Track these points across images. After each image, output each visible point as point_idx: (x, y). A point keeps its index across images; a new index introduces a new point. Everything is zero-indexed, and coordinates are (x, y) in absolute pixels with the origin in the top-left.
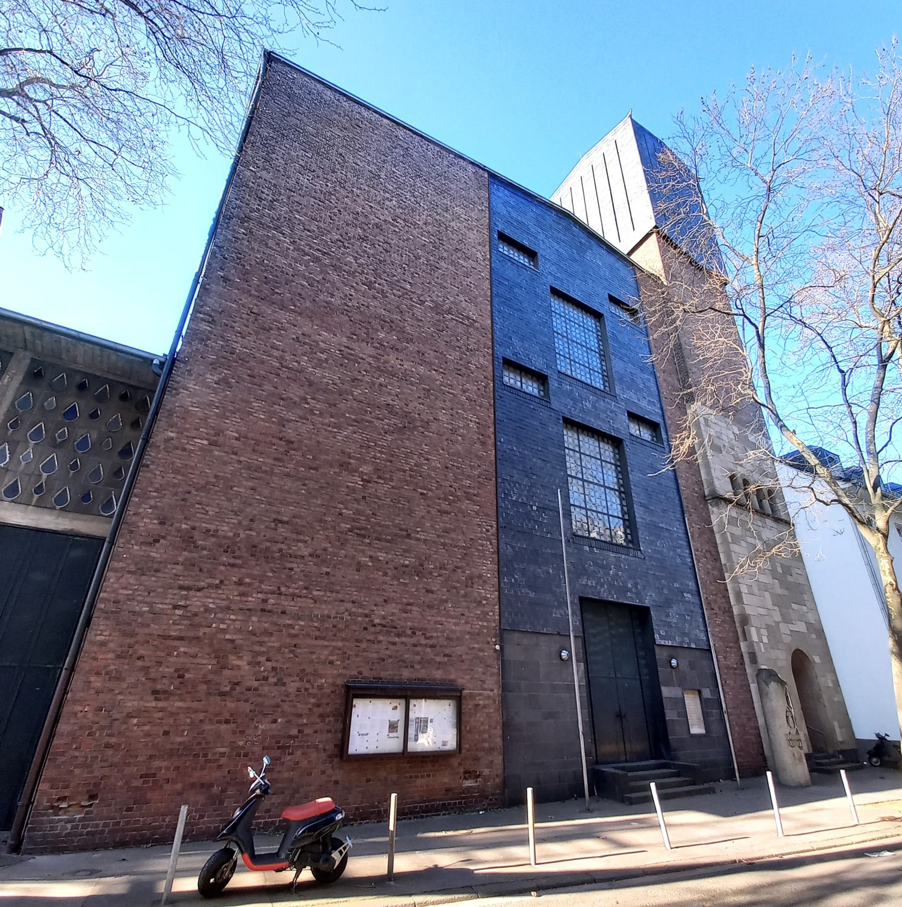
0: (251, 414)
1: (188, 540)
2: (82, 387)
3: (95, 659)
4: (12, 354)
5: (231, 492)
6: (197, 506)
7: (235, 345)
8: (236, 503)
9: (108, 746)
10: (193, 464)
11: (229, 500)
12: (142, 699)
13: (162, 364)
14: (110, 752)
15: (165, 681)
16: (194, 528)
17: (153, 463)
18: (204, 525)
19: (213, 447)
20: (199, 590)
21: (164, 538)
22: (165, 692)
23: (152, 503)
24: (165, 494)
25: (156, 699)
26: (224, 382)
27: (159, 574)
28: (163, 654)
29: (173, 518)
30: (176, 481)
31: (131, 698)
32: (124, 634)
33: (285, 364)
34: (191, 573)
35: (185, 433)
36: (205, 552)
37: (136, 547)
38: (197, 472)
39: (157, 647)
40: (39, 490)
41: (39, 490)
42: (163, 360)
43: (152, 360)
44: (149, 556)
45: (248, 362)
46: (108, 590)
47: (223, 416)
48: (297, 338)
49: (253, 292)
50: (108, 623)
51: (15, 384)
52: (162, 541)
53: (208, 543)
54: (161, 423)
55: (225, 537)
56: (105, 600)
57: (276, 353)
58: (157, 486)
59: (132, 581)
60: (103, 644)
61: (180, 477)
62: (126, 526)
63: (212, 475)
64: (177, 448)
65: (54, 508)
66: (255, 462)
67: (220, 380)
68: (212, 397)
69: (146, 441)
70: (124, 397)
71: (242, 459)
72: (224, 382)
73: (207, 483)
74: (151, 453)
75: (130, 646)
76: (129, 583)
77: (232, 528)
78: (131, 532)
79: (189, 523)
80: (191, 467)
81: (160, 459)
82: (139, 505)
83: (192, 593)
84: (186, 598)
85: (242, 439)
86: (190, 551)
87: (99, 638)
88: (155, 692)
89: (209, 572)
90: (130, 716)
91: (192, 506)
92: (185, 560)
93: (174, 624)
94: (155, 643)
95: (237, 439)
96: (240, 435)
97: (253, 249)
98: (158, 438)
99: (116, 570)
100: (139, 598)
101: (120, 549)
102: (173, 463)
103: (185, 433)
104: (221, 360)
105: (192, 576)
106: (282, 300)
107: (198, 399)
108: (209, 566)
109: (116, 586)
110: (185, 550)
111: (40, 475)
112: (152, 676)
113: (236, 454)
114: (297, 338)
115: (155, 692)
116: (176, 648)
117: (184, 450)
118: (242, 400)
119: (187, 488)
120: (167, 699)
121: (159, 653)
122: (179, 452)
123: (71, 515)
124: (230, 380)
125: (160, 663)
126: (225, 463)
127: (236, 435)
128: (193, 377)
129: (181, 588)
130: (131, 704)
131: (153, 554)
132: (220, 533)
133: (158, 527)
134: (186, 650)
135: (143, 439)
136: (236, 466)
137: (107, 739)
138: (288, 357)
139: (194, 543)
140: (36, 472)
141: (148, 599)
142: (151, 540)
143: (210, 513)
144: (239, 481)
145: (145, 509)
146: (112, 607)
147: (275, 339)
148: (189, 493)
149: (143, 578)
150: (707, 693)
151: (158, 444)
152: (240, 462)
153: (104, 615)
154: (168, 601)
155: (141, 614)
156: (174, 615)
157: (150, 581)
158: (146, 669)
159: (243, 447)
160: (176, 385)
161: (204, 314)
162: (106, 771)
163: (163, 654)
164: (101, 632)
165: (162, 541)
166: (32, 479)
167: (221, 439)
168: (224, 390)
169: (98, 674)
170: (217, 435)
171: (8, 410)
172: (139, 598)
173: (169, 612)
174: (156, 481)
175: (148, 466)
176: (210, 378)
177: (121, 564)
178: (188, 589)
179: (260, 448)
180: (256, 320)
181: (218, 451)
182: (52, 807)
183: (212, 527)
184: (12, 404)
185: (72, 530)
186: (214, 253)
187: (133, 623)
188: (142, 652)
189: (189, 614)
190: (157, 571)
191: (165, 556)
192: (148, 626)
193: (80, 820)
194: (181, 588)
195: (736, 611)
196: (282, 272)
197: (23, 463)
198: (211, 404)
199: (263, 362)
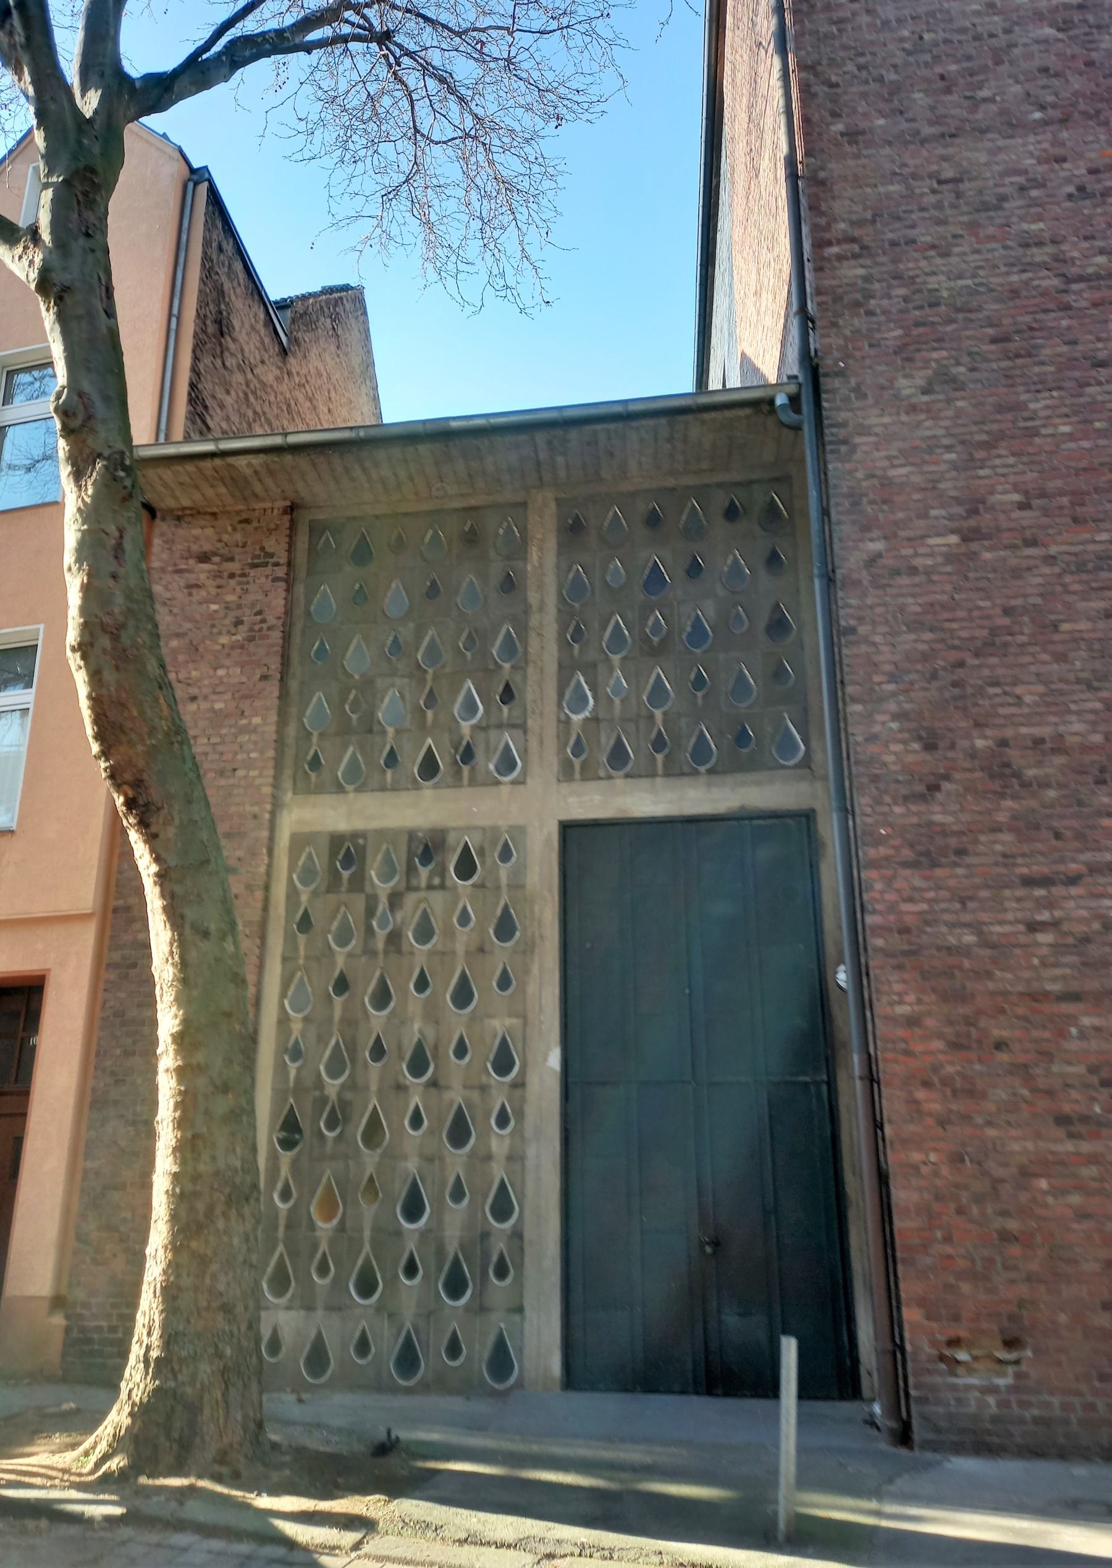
0: (1033, 433)
1: (1001, 772)
2: (653, 520)
3: (908, 1053)
4: (524, 505)
5: (1056, 637)
6: (992, 690)
7: (932, 282)
8: (1080, 660)
9: (1006, 1237)
10: (945, 598)
11: (1061, 658)
12: (1038, 1136)
13: (794, 401)
14: (1015, 1250)
15: (1074, 1094)
16: (1003, 743)
17: (861, 619)
18: (1024, 730)
19: (974, 546)
20: (1073, 880)
21: (947, 777)
22: (1085, 1119)
23: (892, 706)
24: (912, 683)
25: (1071, 1136)
26: (944, 379)
27: (969, 860)
28: (1047, 1034)
29: (950, 730)
30: (922, 647)
31: (1014, 1132)
32: (945, 997)
33: (1074, 271)
34: (1039, 846)
35: (903, 534)
36: (1052, 794)
37: (897, 810)
38: (961, 614)
39: (1026, 1019)
40: (659, 744)
41: (659, 744)
42: (792, 389)
43: (771, 401)
44: (931, 824)
45: (980, 309)
46: (878, 907)
47: (970, 464)
48: (1081, 189)
49: (927, 131)
50: (906, 976)
51: (551, 559)
52: (946, 786)
53: (1048, 770)
54: (844, 528)
55: (1086, 749)
56: (879, 930)
57: (1040, 255)
58: (888, 668)
59: (918, 882)
60: (912, 1021)
61: (929, 636)
62: (862, 769)
63: (998, 611)
64: (897, 572)
65: (695, 773)
66: (1090, 547)
67: (930, 382)
68: (929, 429)
69: (830, 580)
70: (731, 513)
71: (1053, 550)
72: (944, 379)
73: (994, 631)
74: (849, 601)
75: (969, 1022)
76: (915, 889)
77: (1094, 723)
78: (875, 779)
79: (989, 732)
80: (944, 607)
81: (871, 607)
82: (869, 717)
83: (1058, 891)
84: (1050, 905)
85: (1036, 502)
86: (1015, 797)
87: (900, 1010)
88: (1062, 1120)
89: (1080, 836)
90: (1026, 1174)
91: (980, 692)
92: (1014, 818)
93: (1044, 964)
94: (1020, 1011)
95: (1023, 506)
96: (1026, 493)
97: (886, 23)
98: (851, 561)
99: (874, 864)
100: (947, 917)
101: (869, 820)
102: (902, 609)
103: (903, 534)
104: (916, 332)
105: (1042, 854)
106: (1003, 112)
107: (900, 444)
108: (1074, 823)
109: (890, 897)
110: (1002, 795)
111: (651, 717)
112: (1042, 1083)
113: (1033, 543)
114: (1081, 189)
115: (1062, 1120)
116: (1072, 1019)
117: (913, 571)
118: (1000, 409)
119: (954, 656)
120: (1095, 1136)
121: (1036, 1034)
122: (905, 580)
123: (729, 779)
124: (954, 370)
125: (1047, 1056)
126: (1017, 573)
127: (1016, 497)
128: (870, 401)
129: (1029, 882)
130: (1020, 1146)
131: (938, 818)
132: (1071, 740)
133: (927, 756)
134: (1096, 1021)
135: (821, 576)
136: (1047, 570)
137: (998, 1223)
138: (1072, 250)
139: (1017, 775)
140: (643, 712)
141: (967, 918)
142: (920, 788)
143: (1028, 699)
144: (1068, 606)
145: (883, 723)
146: (899, 943)
147: (1022, 219)
148: (961, 664)
149: (938, 872)
151: (855, 576)
152: (1050, 560)
153: (893, 961)
154: (1010, 916)
155: (964, 951)
156: (1038, 944)
157: (953, 876)
158: (1022, 1070)
159: (1044, 520)
160: (842, 433)
161: (839, 242)
162: (1023, 1290)
163: (1047, 1034)
164: (898, 998)
165: (946, 786)
166: (642, 726)
167: (986, 520)
168: (949, 401)
169: (927, 1084)
170: (974, 512)
171: (559, 611)
172: (947, 917)
173: (1023, 939)
174: (881, 658)
175: (852, 630)
176: (907, 386)
177: (883, 851)
178: (1046, 882)
179: (1088, 510)
180: (959, 195)
181: (988, 550)
182: (942, 1358)
183: (1045, 731)
184: (561, 599)
185: (742, 808)
186: (806, 90)
187: (957, 972)
188: (996, 1033)
189: (1070, 940)
190: (961, 852)
191: (965, 817)
192: (989, 975)
193: (1011, 1389)
194: (1029, 882)
196: (977, 38)
197: (617, 701)
198: (932, 446)
199: (1015, 293)
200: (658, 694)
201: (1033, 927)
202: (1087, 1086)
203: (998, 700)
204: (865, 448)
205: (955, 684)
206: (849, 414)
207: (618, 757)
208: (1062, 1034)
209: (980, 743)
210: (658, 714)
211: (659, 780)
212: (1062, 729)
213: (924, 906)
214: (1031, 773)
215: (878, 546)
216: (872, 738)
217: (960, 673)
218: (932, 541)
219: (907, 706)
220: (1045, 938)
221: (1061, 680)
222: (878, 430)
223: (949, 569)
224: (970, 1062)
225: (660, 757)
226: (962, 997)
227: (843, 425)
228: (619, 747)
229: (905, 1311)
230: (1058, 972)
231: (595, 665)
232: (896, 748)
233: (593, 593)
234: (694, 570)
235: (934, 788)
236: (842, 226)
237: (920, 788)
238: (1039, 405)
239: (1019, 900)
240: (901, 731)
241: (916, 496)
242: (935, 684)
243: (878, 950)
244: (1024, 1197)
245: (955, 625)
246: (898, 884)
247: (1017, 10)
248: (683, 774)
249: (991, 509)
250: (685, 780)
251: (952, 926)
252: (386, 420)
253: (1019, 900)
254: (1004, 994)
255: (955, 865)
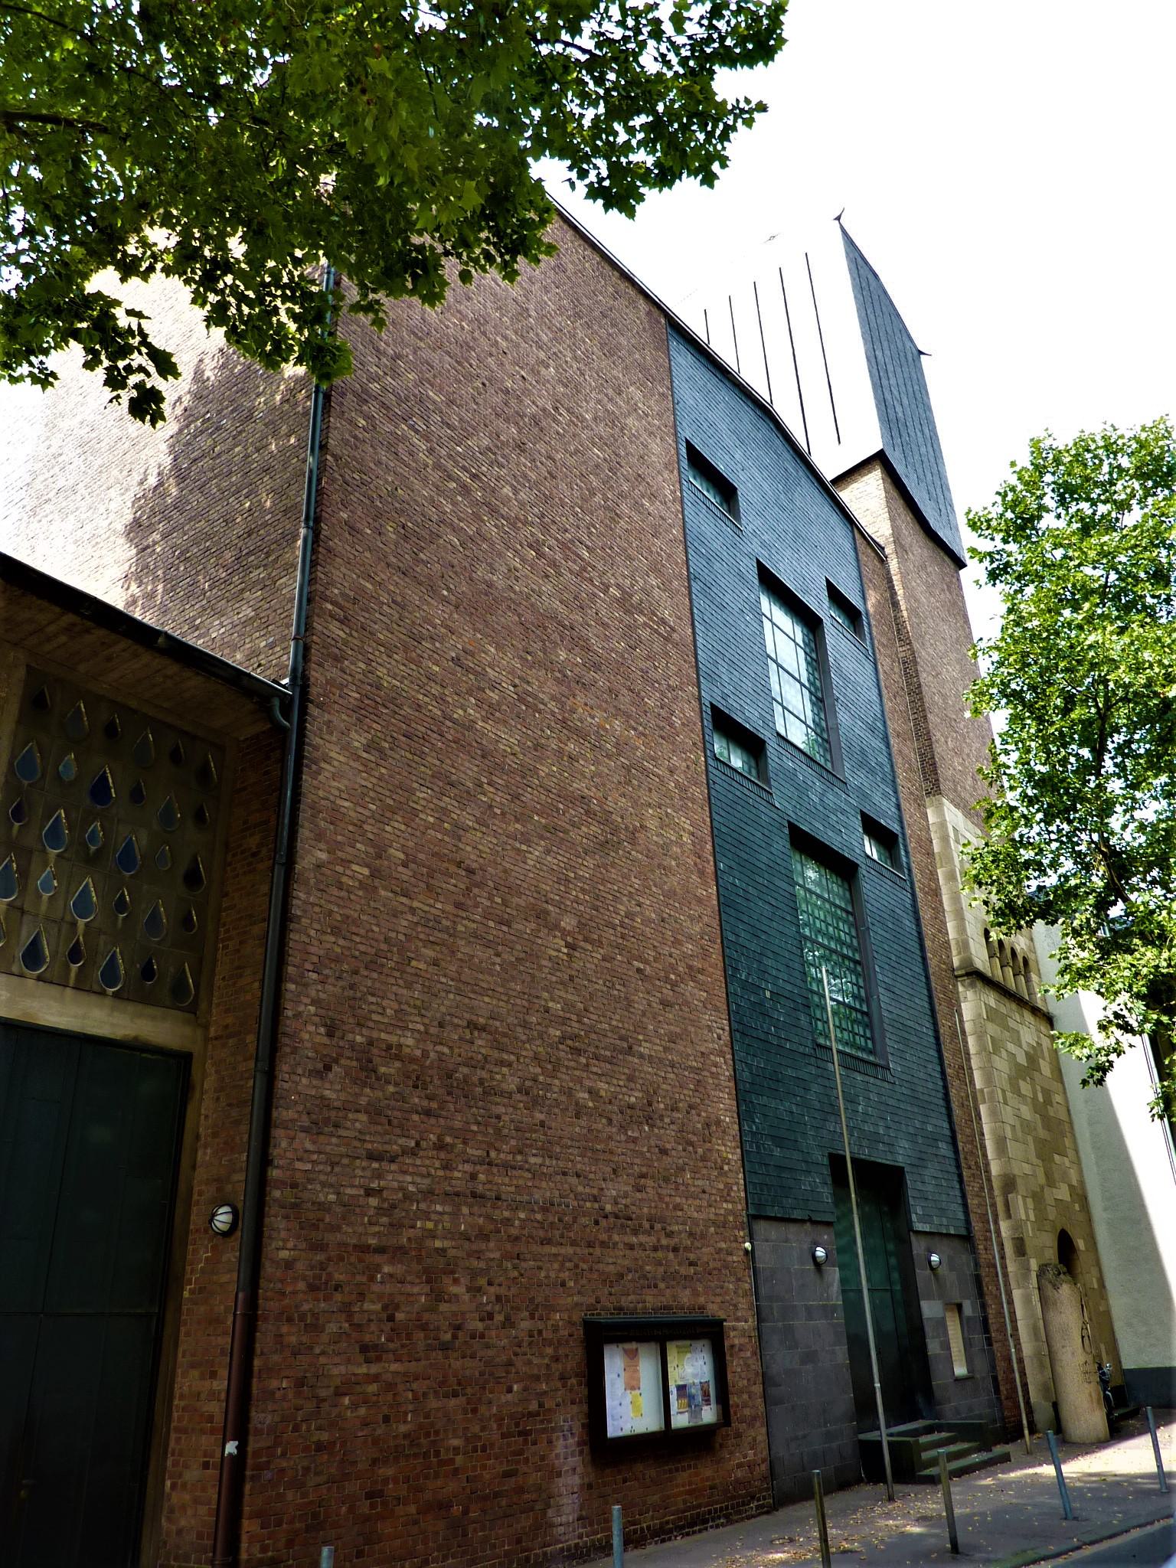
11: (409, 986)
37: (304, 1081)
38: (362, 932)
41: (74, 955)
52: (336, 1068)
56: (281, 1184)
59: (309, 1146)
60: (289, 1264)
63: (382, 938)
65: (103, 993)
71: (415, 904)
79: (365, 1031)
88: (364, 1349)
100: (322, 1178)
110: (365, 1085)
111: (74, 924)
116: (378, 1268)
123: (131, 1007)
125: (362, 1296)
133: (326, 1040)
140: (68, 918)
141: (333, 1179)
150: (968, 1309)
185: (136, 1038)
189: (386, 1205)
191: (343, 1096)
192: (338, 1228)
194: (371, 1156)
195: (995, 1169)
197: (46, 896)
200: (83, 906)
201: (369, 1192)
202: (380, 1320)
203: (373, 1007)
204: (326, 774)
205: (352, 987)
206: (321, 742)
207: (32, 956)
208: (372, 1279)
209: (359, 1039)
210: (81, 923)
211: (68, 991)
212: (402, 1040)
213: (309, 1167)
214: (383, 1070)
215: (323, 856)
216: (298, 1015)
217: (357, 979)
218: (355, 867)
219: (322, 996)
220: (373, 1202)
221: (407, 1003)
222: (336, 763)
223: (361, 893)
224: (318, 1300)
225: (74, 967)
226: (318, 1247)
227: (316, 748)
228: (35, 945)
229: (245, 1523)
230: (377, 1229)
231: (31, 852)
232: (312, 1028)
233: (43, 776)
234: (137, 796)
235: (328, 1068)
236: (336, 591)
237: (320, 1066)
238: (422, 795)
239: (364, 1169)
240: (316, 1015)
241: (351, 828)
242: (341, 983)
243: (275, 1200)
244: (335, 1412)
245: (358, 939)
246: (296, 1144)
247: (539, 630)
248: (90, 991)
249: (388, 859)
250: (93, 998)
251: (324, 1185)
252: (1128, 1364)
253: (364, 1169)
254: (346, 1245)
255: (332, 1135)
